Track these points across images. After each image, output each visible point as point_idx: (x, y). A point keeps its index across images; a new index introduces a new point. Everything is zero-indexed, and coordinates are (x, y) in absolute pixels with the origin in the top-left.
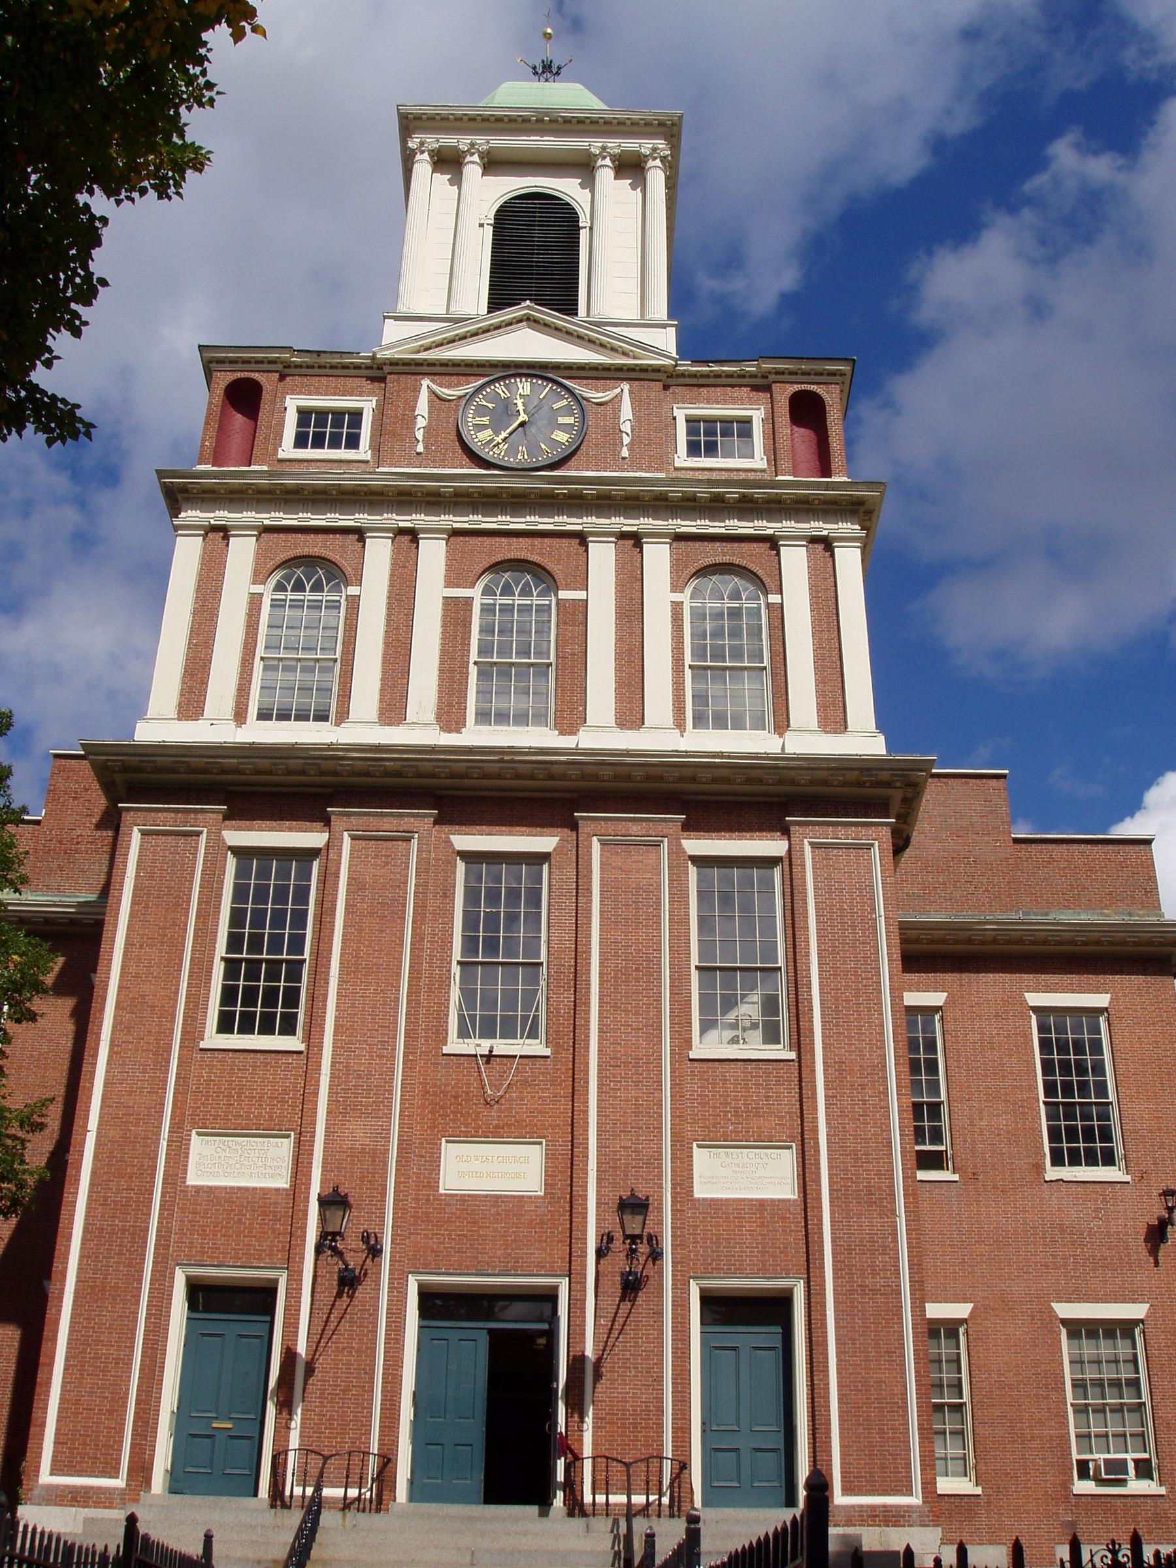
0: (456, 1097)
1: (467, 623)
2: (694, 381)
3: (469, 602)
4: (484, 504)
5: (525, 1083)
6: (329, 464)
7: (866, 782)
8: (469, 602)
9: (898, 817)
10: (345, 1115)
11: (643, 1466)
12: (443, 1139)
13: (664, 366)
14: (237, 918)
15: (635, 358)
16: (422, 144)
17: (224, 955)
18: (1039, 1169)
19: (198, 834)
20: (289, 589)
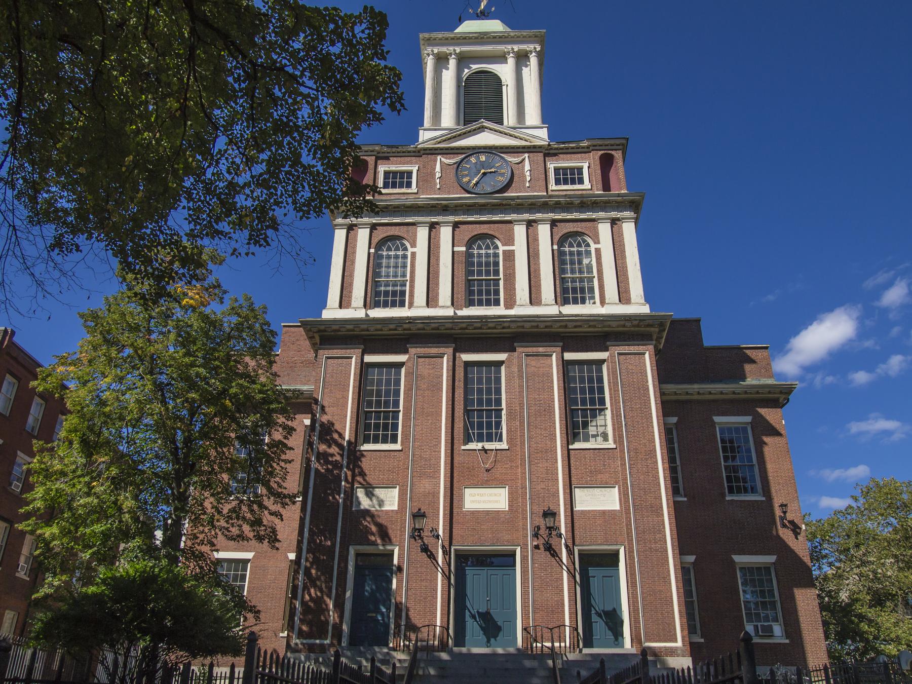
4: (406, 211)
9: (656, 340)
11: (557, 630)
18: (723, 495)
19: (351, 358)
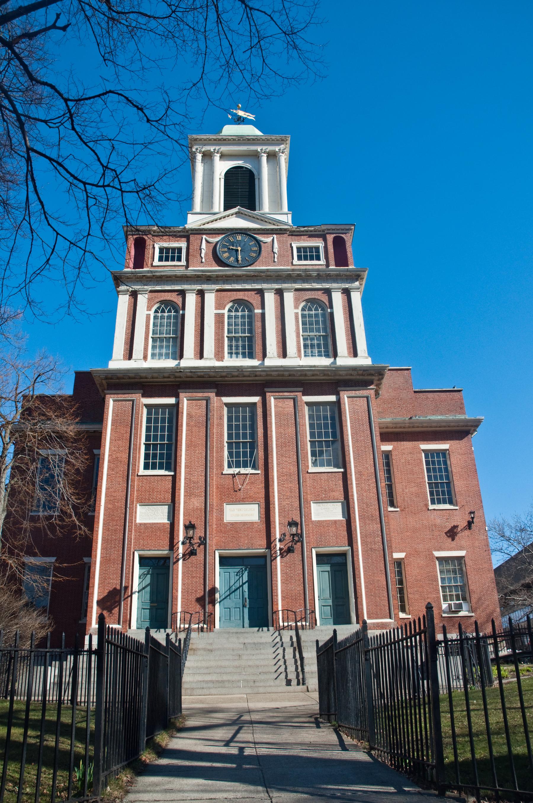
0: (228, 489)
1: (223, 322)
2: (298, 233)
3: (223, 315)
8: (223, 315)
10: (190, 496)
14: (148, 429)
15: (277, 226)
16: (197, 149)
18: (427, 505)
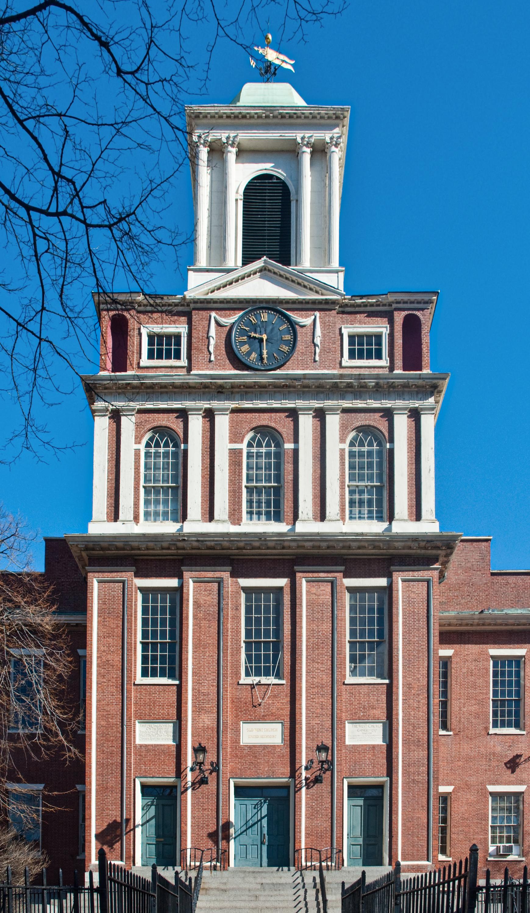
1: (240, 464)
5: (275, 696)
6: (167, 370)
7: (429, 547)
10: (199, 712)
12: (241, 722)
13: (337, 300)
15: (322, 294)
17: (141, 640)
18: (487, 729)
20: (153, 446)
